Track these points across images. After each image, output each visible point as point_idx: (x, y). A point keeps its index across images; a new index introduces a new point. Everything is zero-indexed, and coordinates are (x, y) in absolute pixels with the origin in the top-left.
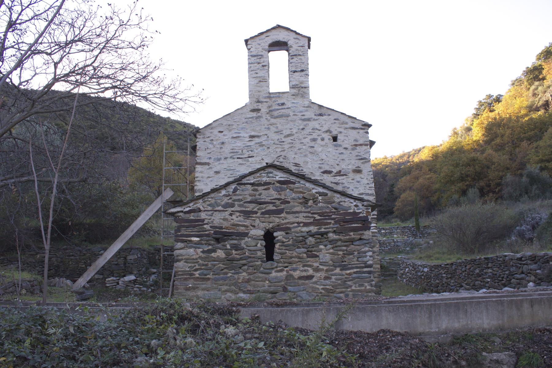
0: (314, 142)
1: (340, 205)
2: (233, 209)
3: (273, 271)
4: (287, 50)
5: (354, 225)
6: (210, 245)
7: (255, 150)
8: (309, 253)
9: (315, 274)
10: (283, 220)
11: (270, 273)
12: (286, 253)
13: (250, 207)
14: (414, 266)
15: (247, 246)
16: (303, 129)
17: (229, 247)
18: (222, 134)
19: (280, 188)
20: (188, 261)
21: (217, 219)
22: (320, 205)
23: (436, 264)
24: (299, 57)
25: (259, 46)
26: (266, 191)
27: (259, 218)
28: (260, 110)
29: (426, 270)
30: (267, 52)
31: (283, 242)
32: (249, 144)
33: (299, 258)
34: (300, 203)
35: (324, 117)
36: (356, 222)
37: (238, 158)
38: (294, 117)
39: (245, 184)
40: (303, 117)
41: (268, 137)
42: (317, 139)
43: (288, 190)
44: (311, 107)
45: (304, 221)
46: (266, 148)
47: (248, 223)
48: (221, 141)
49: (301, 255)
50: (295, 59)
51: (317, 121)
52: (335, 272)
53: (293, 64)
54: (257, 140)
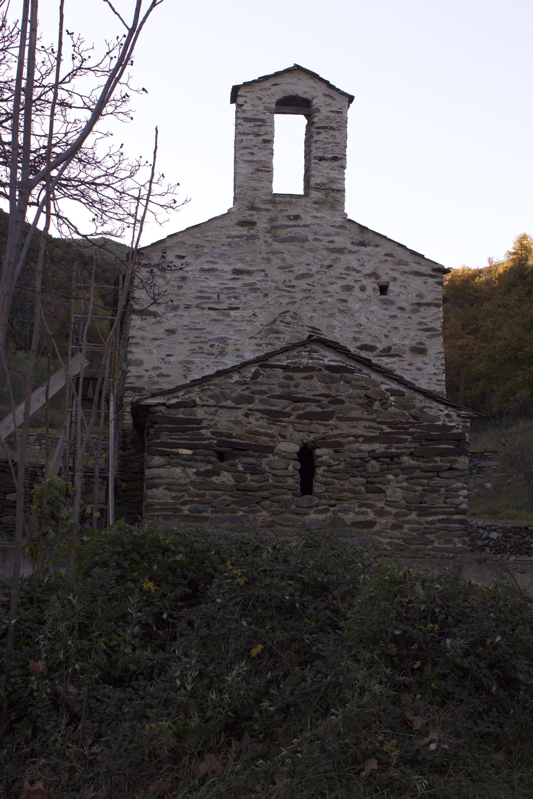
0: (347, 293)
1: (423, 412)
2: (250, 406)
5: (442, 446)
6: (209, 462)
7: (242, 297)
8: (369, 485)
9: (378, 519)
10: (332, 430)
11: (307, 514)
12: (334, 483)
13: (280, 405)
15: (272, 468)
16: (330, 267)
17: (242, 469)
19: (330, 377)
20: (172, 487)
21: (224, 421)
23: (517, 525)
24: (331, 132)
25: (259, 102)
26: (307, 381)
27: (293, 423)
28: (255, 223)
29: (494, 535)
31: (330, 466)
32: (232, 284)
33: (354, 492)
34: (361, 405)
35: (368, 249)
37: (210, 309)
38: (315, 243)
40: (331, 246)
41: (266, 275)
42: (354, 287)
43: (342, 382)
44: (345, 228)
45: (365, 434)
46: (261, 295)
47: (274, 430)
49: (358, 488)
53: (319, 145)
54: (247, 279)
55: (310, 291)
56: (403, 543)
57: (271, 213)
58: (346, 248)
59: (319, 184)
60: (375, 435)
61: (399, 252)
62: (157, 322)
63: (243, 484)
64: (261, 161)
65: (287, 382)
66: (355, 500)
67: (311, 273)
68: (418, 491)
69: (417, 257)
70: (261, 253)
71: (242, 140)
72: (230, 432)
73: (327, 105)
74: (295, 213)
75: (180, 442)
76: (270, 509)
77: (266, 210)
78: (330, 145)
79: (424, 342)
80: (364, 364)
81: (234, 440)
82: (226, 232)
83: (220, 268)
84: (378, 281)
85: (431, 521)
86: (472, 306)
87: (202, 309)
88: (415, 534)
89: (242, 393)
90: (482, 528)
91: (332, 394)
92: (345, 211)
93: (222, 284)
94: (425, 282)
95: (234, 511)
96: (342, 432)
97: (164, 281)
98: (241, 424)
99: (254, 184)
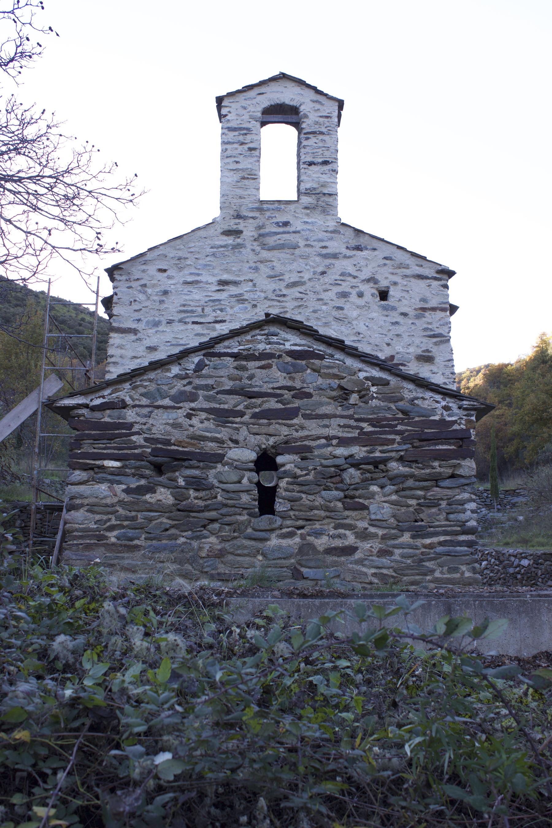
0: (343, 300)
1: (414, 405)
2: (193, 405)
3: (273, 536)
4: (297, 125)
5: (441, 447)
6: (142, 476)
7: (228, 309)
8: (348, 500)
9: (359, 544)
10: (297, 431)
12: (301, 498)
13: (230, 402)
14: (499, 557)
16: (323, 273)
17: (183, 483)
18: (165, 275)
19: (293, 365)
20: (96, 509)
21: (160, 424)
22: (374, 403)
24: (321, 137)
25: (244, 112)
26: (263, 371)
28: (241, 232)
29: (525, 562)
30: (258, 124)
31: (295, 477)
32: (217, 296)
33: (328, 509)
34: (334, 398)
35: (365, 253)
36: (446, 440)
37: (194, 323)
38: (307, 249)
39: (220, 355)
40: (324, 251)
41: (254, 285)
42: (350, 293)
43: (309, 371)
44: (339, 233)
45: (340, 435)
46: (249, 306)
47: (223, 433)
48: (163, 288)
49: (332, 505)
50: (313, 140)
51: (351, 261)
52: (401, 540)
53: (308, 150)
54: (233, 290)
55: (302, 299)
56: (394, 574)
57: (258, 220)
58: (340, 253)
59: (309, 189)
60: (353, 435)
61: (399, 256)
62: (137, 340)
63: (184, 503)
64: (247, 169)
65: (239, 373)
66: (330, 520)
67: (303, 280)
68: (411, 506)
69: (419, 259)
70: (248, 262)
71: (226, 150)
72: (168, 438)
73: (316, 111)
74: (285, 219)
75: (105, 451)
76: (220, 534)
77: (253, 218)
78: (320, 150)
79: (430, 349)
80: (336, 348)
81: (173, 447)
82: (210, 242)
83: (204, 280)
84: (377, 286)
85: (430, 544)
86: (506, 386)
87: (185, 323)
88: (409, 561)
89: (183, 388)
90: (513, 556)
91: (295, 385)
92: (339, 215)
93: (206, 296)
94: (429, 286)
95: (175, 537)
96: (310, 433)
97: (144, 296)
98: (181, 427)
99: (240, 192)
